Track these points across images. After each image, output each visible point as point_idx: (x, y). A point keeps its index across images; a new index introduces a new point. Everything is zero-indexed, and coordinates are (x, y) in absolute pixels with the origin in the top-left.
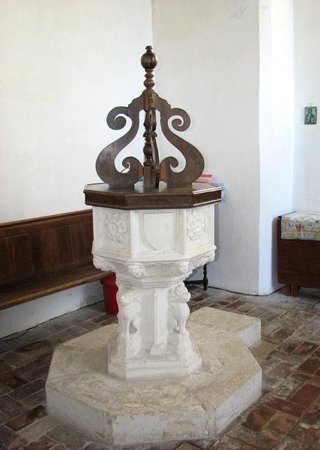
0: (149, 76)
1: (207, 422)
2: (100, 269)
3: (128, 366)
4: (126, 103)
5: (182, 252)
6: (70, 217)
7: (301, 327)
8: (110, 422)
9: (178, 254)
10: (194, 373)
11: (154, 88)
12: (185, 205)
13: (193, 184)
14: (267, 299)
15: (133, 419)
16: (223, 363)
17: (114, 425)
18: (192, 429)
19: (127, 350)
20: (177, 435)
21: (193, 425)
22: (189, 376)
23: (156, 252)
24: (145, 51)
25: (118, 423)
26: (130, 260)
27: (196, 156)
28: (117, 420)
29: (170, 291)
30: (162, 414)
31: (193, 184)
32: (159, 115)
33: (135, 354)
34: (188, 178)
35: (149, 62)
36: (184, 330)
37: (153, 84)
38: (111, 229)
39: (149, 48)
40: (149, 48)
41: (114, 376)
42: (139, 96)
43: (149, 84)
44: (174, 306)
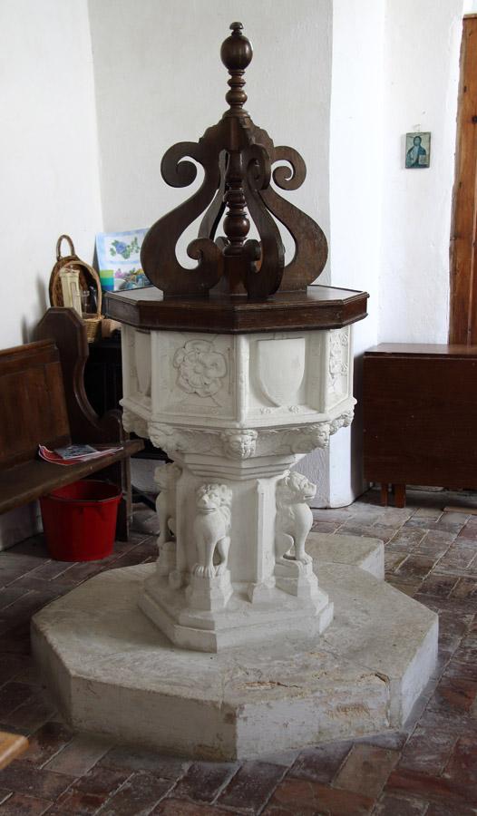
0: (236, 84)
1: (389, 705)
2: (160, 449)
3: (218, 626)
4: (195, 136)
5: (320, 408)
6: (190, 328)
7: (441, 555)
8: (231, 718)
9: (314, 412)
10: (326, 630)
11: (245, 107)
12: (330, 324)
13: (309, 287)
14: (345, 513)
15: (271, 707)
16: (366, 612)
17: (240, 724)
18: (360, 720)
19: (212, 597)
20: (341, 731)
21: (366, 711)
22: (322, 636)
23: (277, 409)
24: (229, 33)
25: (245, 719)
26: (238, 426)
27: (315, 237)
28: (245, 714)
29: (279, 483)
30: (318, 694)
31: (309, 287)
32: (220, 163)
33: (225, 603)
34: (299, 277)
35: (236, 55)
36: (303, 554)
37: (244, 100)
38: (190, 373)
39: (236, 27)
40: (236, 27)
41: (188, 648)
42: (216, 123)
43: (235, 97)
44: (288, 510)
